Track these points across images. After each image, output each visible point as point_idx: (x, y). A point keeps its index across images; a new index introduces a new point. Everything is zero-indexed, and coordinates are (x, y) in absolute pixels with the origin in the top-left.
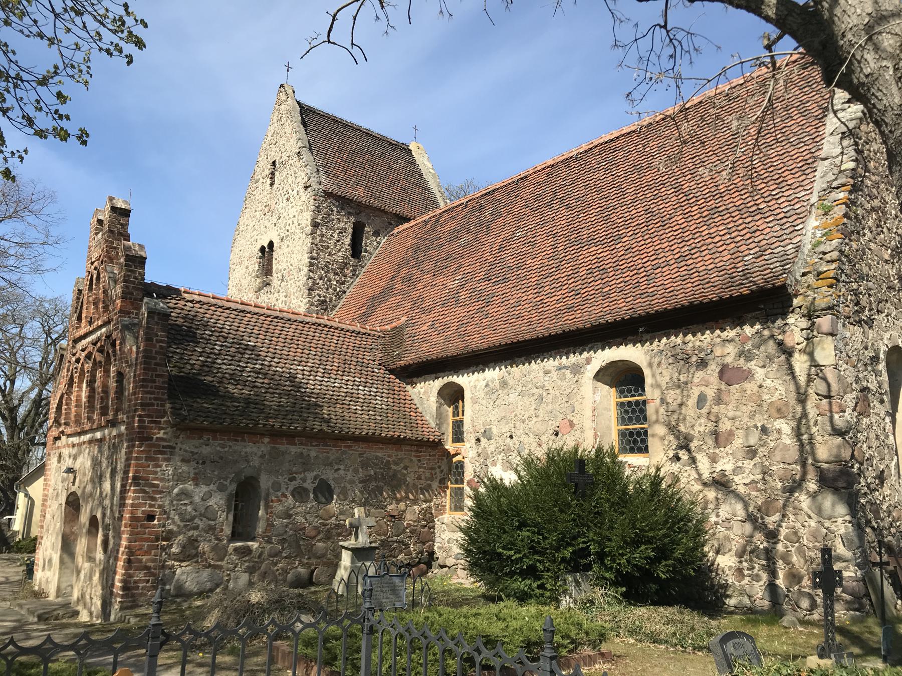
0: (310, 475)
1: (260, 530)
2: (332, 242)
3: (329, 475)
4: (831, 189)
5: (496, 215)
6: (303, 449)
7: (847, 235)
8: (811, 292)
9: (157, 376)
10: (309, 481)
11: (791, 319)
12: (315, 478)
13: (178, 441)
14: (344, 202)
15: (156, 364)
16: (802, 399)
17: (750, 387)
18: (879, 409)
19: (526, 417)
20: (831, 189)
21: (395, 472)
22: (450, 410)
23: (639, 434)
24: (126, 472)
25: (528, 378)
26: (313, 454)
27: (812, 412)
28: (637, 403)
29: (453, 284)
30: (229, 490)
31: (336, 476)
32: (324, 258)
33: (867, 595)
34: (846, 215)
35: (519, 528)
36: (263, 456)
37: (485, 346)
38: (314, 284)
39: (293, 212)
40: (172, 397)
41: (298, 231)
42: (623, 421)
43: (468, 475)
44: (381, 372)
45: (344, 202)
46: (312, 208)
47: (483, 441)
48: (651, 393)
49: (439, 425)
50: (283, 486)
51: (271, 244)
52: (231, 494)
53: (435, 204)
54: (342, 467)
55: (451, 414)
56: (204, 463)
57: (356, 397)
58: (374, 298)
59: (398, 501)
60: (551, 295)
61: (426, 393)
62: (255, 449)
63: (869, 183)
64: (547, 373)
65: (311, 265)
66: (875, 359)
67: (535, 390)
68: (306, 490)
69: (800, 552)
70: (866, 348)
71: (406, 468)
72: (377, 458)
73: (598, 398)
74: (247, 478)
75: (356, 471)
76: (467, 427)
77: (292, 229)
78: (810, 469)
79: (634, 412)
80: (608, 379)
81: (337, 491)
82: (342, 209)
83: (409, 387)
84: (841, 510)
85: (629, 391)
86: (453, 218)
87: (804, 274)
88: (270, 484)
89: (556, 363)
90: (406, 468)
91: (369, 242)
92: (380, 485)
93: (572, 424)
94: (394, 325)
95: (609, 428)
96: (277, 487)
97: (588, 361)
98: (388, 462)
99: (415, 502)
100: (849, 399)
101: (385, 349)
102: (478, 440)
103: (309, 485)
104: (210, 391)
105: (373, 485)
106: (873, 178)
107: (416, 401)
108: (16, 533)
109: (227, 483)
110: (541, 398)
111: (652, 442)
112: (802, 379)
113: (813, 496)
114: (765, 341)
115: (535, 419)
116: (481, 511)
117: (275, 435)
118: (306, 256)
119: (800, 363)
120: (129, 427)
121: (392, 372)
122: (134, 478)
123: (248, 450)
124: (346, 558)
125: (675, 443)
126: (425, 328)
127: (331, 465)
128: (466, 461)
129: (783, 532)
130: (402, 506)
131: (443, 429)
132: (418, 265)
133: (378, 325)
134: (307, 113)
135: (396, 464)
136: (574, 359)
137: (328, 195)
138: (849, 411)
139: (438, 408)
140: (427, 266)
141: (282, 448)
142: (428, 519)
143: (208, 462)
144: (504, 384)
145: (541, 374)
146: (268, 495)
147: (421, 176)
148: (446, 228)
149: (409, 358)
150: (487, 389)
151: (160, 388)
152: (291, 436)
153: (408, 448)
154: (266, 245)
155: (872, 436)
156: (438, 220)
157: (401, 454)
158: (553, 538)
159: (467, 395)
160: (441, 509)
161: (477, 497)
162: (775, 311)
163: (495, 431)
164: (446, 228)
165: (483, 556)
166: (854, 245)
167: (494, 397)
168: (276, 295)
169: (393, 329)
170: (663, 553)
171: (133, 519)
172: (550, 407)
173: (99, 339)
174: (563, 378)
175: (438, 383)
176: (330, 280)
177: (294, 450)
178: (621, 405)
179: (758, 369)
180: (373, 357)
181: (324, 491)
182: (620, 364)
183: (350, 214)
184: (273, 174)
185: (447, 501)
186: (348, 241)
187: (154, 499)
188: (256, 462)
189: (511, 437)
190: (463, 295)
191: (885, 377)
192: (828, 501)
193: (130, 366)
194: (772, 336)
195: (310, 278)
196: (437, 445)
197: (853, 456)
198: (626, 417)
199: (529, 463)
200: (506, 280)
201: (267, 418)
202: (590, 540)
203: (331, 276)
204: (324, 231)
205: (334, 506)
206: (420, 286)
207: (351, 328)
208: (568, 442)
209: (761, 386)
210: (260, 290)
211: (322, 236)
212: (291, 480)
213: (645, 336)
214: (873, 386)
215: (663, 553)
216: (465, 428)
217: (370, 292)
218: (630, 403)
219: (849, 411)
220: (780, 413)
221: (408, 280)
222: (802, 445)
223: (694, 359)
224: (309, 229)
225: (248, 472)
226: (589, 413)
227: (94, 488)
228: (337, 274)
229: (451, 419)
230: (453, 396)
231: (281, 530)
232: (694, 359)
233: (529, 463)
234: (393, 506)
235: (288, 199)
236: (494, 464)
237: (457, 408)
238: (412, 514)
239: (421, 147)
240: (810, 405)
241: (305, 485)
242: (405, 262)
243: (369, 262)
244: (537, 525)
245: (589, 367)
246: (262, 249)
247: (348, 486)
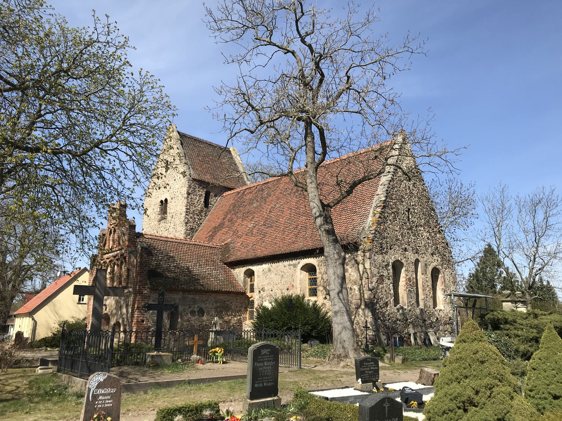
1: (179, 326)
3: (203, 306)
4: (377, 207)
5: (269, 195)
7: (379, 223)
8: (366, 245)
11: (359, 253)
14: (201, 183)
16: (361, 279)
20: (377, 207)
21: (228, 305)
22: (249, 279)
24: (133, 305)
25: (279, 268)
26: (197, 298)
27: (364, 283)
29: (251, 226)
32: (192, 209)
33: (376, 340)
34: (380, 217)
35: (271, 321)
36: (180, 299)
37: (262, 255)
38: (188, 220)
39: (177, 186)
40: (149, 278)
41: (180, 196)
43: (256, 305)
44: (220, 264)
45: (201, 183)
46: (187, 186)
48: (318, 275)
49: (245, 286)
50: (187, 310)
51: (166, 200)
55: (249, 281)
57: (211, 274)
58: (215, 228)
59: (229, 316)
60: (287, 236)
61: (239, 273)
63: (392, 203)
64: (285, 266)
65: (187, 212)
66: (387, 265)
68: (195, 311)
69: (359, 328)
70: (384, 262)
71: (231, 303)
73: (302, 276)
75: (213, 304)
76: (255, 287)
77: (177, 194)
78: (363, 301)
79: (313, 282)
80: (306, 269)
81: (206, 312)
82: (201, 186)
83: (232, 270)
84: (370, 314)
86: (251, 193)
87: (364, 238)
89: (288, 263)
90: (231, 303)
91: (212, 200)
92: (222, 309)
93: (293, 286)
94: (225, 242)
95: (306, 288)
96: (184, 310)
97: (299, 263)
99: (235, 316)
100: (375, 279)
101: (223, 255)
102: (260, 292)
103: (196, 310)
104: (160, 275)
105: (219, 310)
106: (394, 201)
107: (235, 276)
108: (27, 339)
110: (282, 276)
111: (319, 293)
112: (361, 273)
113: (363, 310)
114: (351, 260)
116: (259, 317)
117: (184, 291)
118: (184, 208)
119: (361, 267)
120: (134, 289)
121: (225, 264)
122: (138, 307)
123: (175, 297)
124: (212, 335)
125: (325, 293)
126: (239, 245)
128: (255, 300)
129: (355, 321)
130: (230, 317)
131: (246, 287)
132: (236, 214)
133: (217, 242)
134: (182, 136)
135: (228, 301)
136: (294, 262)
137: (194, 180)
138: (374, 283)
139: (244, 279)
140: (239, 215)
142: (240, 323)
144: (270, 270)
146: (182, 313)
147: (235, 164)
148: (248, 197)
149: (232, 259)
152: (189, 291)
154: (163, 200)
155: (383, 290)
156: (244, 193)
157: (229, 298)
158: (281, 324)
159: (256, 274)
160: (245, 319)
161: (258, 314)
163: (266, 288)
164: (248, 197)
165: (257, 328)
166: (382, 227)
167: (266, 275)
168: (169, 224)
169: (225, 244)
170: (314, 328)
171: (138, 322)
172: (286, 280)
173: (117, 255)
174: (290, 269)
175: (244, 269)
176: (195, 218)
177: (190, 296)
178: (310, 279)
180: (217, 258)
181: (201, 312)
183: (204, 188)
185: (248, 316)
186: (203, 200)
187: (144, 315)
190: (255, 231)
191: (391, 271)
192: (367, 311)
193: (134, 267)
194: (354, 258)
195: (186, 218)
196: (244, 294)
197: (374, 297)
199: (276, 300)
200: (272, 227)
201: (181, 285)
202: (292, 324)
203: (196, 216)
204: (192, 196)
205: (205, 318)
206: (236, 224)
207: (208, 245)
208: (290, 293)
210: (160, 221)
211: (191, 198)
212: (190, 307)
213: (317, 255)
214: (385, 274)
215: (314, 328)
217: (213, 225)
219: (374, 283)
220: (355, 283)
221: (231, 220)
222: (361, 294)
224: (186, 195)
226: (299, 282)
227: (117, 311)
228: (147, 137)
229: (249, 283)
230: (250, 274)
231: (186, 326)
233: (276, 300)
234: (227, 317)
235: (175, 180)
236: (265, 301)
237: (251, 279)
238: (234, 320)
239: (236, 149)
240: (363, 281)
242: (230, 211)
243: (212, 210)
244: (276, 320)
246: (162, 202)
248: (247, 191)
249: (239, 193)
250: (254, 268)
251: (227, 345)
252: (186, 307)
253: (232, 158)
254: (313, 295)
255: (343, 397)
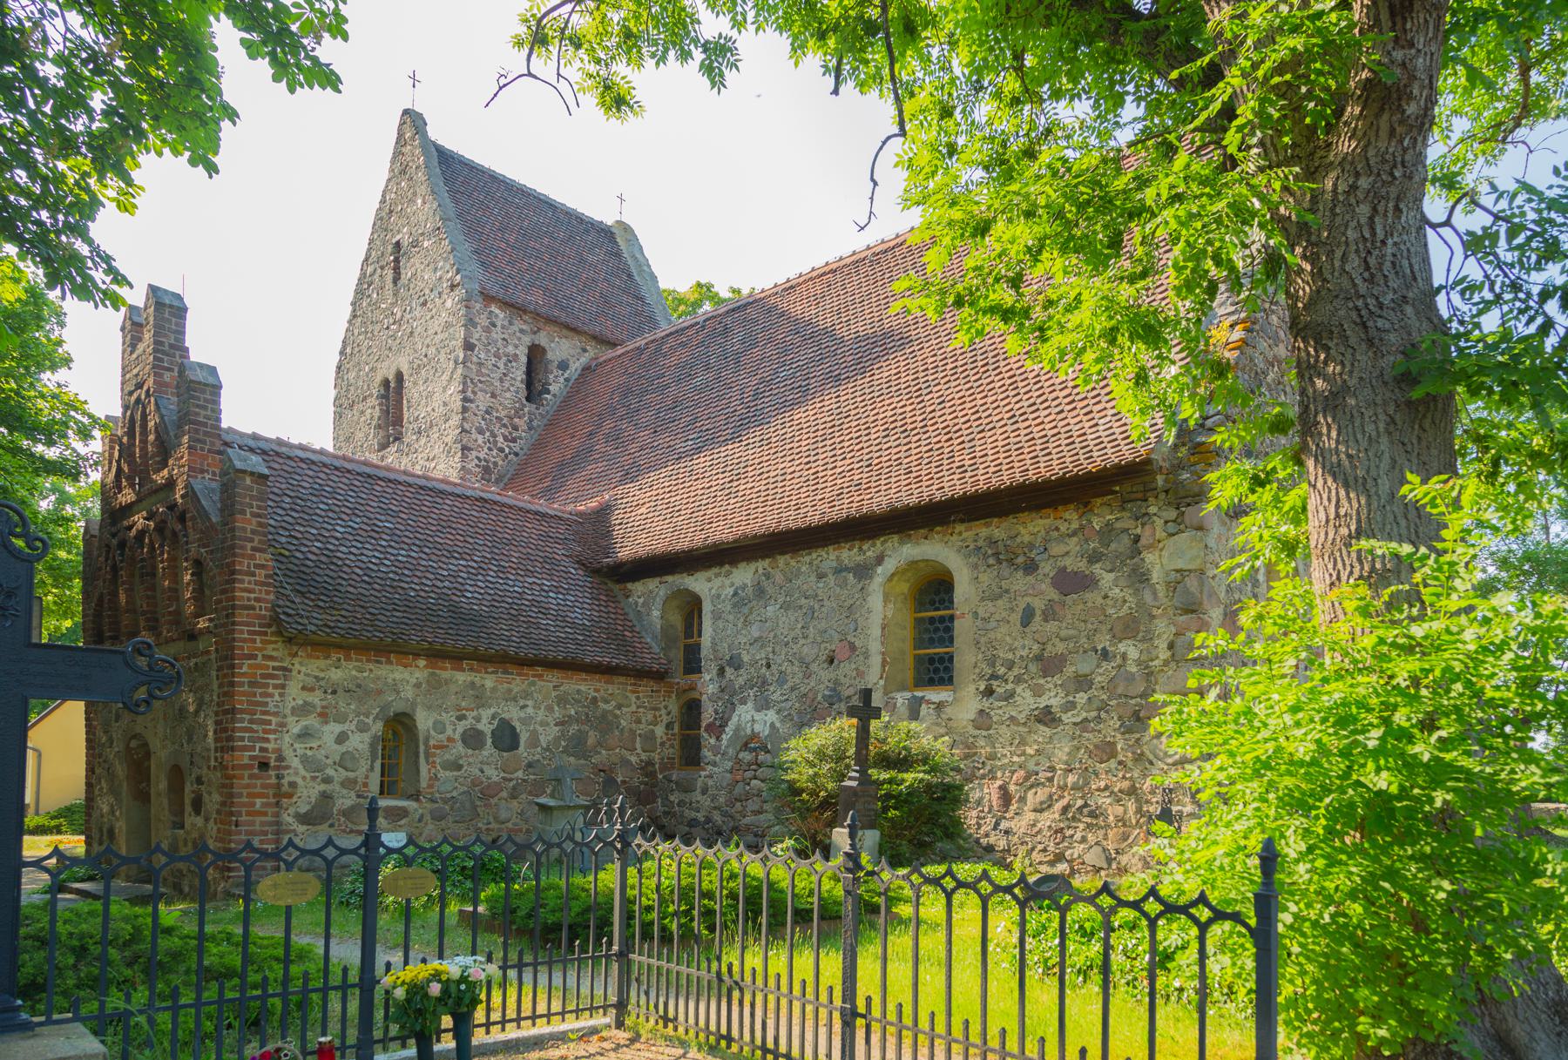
0: (486, 714)
2: (497, 375)
6: (476, 678)
9: (256, 566)
10: (484, 721)
12: (493, 717)
13: (296, 660)
15: (253, 549)
17: (1093, 598)
18: (123, 291)
19: (789, 638)
21: (605, 712)
23: (941, 660)
28: (942, 619)
30: (373, 730)
31: (522, 715)
36: (418, 685)
42: (919, 643)
47: (729, 671)
52: (375, 737)
53: (652, 323)
54: (530, 703)
56: (334, 692)
62: (406, 675)
67: (803, 601)
72: (579, 691)
74: (397, 715)
75: (550, 709)
85: (932, 603)
88: (430, 723)
97: (880, 560)
98: (595, 698)
103: (486, 727)
109: (370, 721)
115: (802, 641)
117: (436, 655)
123: (397, 676)
127: (515, 699)
135: (607, 702)
141: (445, 674)
143: (340, 691)
144: (760, 592)
145: (813, 578)
150: (736, 599)
151: (263, 584)
153: (622, 679)
157: (611, 689)
159: (707, 607)
162: (1134, 496)
163: (746, 658)
172: (823, 625)
174: (843, 584)
177: (462, 677)
179: (1105, 574)
182: (922, 565)
184: (397, 260)
188: (408, 692)
189: (768, 666)
198: (926, 636)
206: (633, 448)
209: (1106, 597)
212: (461, 718)
216: (704, 653)
218: (932, 620)
223: (1021, 560)
225: (399, 707)
226: (876, 632)
228: (505, 426)
232: (1021, 560)
235: (424, 304)
241: (480, 727)
245: (879, 570)
247: (540, 729)
248: (671, 342)
249: (640, 350)
250: (699, 583)
251: (1419, 1048)
252: (448, 717)
253: (618, 255)
254: (931, 683)
255: (88, 740)
